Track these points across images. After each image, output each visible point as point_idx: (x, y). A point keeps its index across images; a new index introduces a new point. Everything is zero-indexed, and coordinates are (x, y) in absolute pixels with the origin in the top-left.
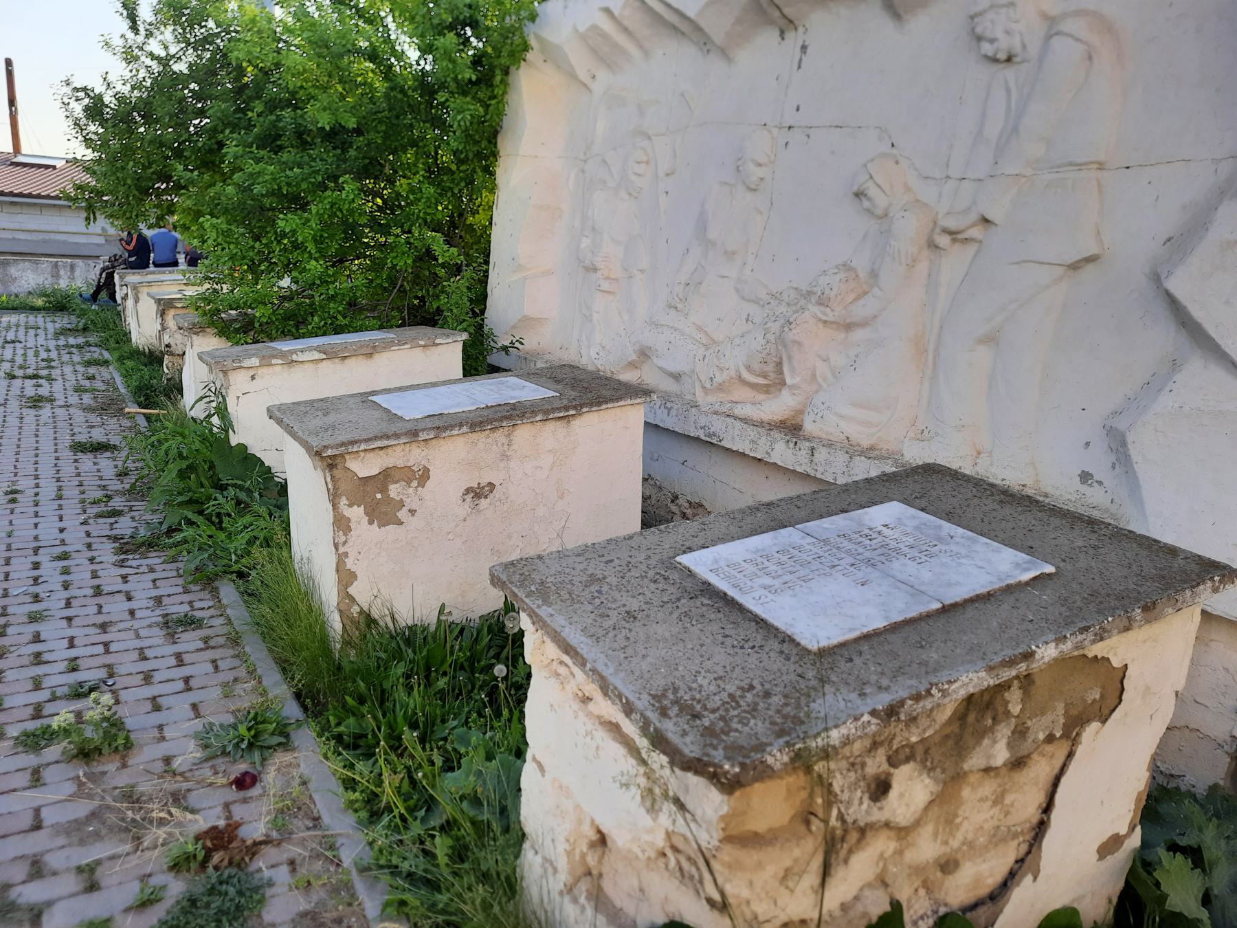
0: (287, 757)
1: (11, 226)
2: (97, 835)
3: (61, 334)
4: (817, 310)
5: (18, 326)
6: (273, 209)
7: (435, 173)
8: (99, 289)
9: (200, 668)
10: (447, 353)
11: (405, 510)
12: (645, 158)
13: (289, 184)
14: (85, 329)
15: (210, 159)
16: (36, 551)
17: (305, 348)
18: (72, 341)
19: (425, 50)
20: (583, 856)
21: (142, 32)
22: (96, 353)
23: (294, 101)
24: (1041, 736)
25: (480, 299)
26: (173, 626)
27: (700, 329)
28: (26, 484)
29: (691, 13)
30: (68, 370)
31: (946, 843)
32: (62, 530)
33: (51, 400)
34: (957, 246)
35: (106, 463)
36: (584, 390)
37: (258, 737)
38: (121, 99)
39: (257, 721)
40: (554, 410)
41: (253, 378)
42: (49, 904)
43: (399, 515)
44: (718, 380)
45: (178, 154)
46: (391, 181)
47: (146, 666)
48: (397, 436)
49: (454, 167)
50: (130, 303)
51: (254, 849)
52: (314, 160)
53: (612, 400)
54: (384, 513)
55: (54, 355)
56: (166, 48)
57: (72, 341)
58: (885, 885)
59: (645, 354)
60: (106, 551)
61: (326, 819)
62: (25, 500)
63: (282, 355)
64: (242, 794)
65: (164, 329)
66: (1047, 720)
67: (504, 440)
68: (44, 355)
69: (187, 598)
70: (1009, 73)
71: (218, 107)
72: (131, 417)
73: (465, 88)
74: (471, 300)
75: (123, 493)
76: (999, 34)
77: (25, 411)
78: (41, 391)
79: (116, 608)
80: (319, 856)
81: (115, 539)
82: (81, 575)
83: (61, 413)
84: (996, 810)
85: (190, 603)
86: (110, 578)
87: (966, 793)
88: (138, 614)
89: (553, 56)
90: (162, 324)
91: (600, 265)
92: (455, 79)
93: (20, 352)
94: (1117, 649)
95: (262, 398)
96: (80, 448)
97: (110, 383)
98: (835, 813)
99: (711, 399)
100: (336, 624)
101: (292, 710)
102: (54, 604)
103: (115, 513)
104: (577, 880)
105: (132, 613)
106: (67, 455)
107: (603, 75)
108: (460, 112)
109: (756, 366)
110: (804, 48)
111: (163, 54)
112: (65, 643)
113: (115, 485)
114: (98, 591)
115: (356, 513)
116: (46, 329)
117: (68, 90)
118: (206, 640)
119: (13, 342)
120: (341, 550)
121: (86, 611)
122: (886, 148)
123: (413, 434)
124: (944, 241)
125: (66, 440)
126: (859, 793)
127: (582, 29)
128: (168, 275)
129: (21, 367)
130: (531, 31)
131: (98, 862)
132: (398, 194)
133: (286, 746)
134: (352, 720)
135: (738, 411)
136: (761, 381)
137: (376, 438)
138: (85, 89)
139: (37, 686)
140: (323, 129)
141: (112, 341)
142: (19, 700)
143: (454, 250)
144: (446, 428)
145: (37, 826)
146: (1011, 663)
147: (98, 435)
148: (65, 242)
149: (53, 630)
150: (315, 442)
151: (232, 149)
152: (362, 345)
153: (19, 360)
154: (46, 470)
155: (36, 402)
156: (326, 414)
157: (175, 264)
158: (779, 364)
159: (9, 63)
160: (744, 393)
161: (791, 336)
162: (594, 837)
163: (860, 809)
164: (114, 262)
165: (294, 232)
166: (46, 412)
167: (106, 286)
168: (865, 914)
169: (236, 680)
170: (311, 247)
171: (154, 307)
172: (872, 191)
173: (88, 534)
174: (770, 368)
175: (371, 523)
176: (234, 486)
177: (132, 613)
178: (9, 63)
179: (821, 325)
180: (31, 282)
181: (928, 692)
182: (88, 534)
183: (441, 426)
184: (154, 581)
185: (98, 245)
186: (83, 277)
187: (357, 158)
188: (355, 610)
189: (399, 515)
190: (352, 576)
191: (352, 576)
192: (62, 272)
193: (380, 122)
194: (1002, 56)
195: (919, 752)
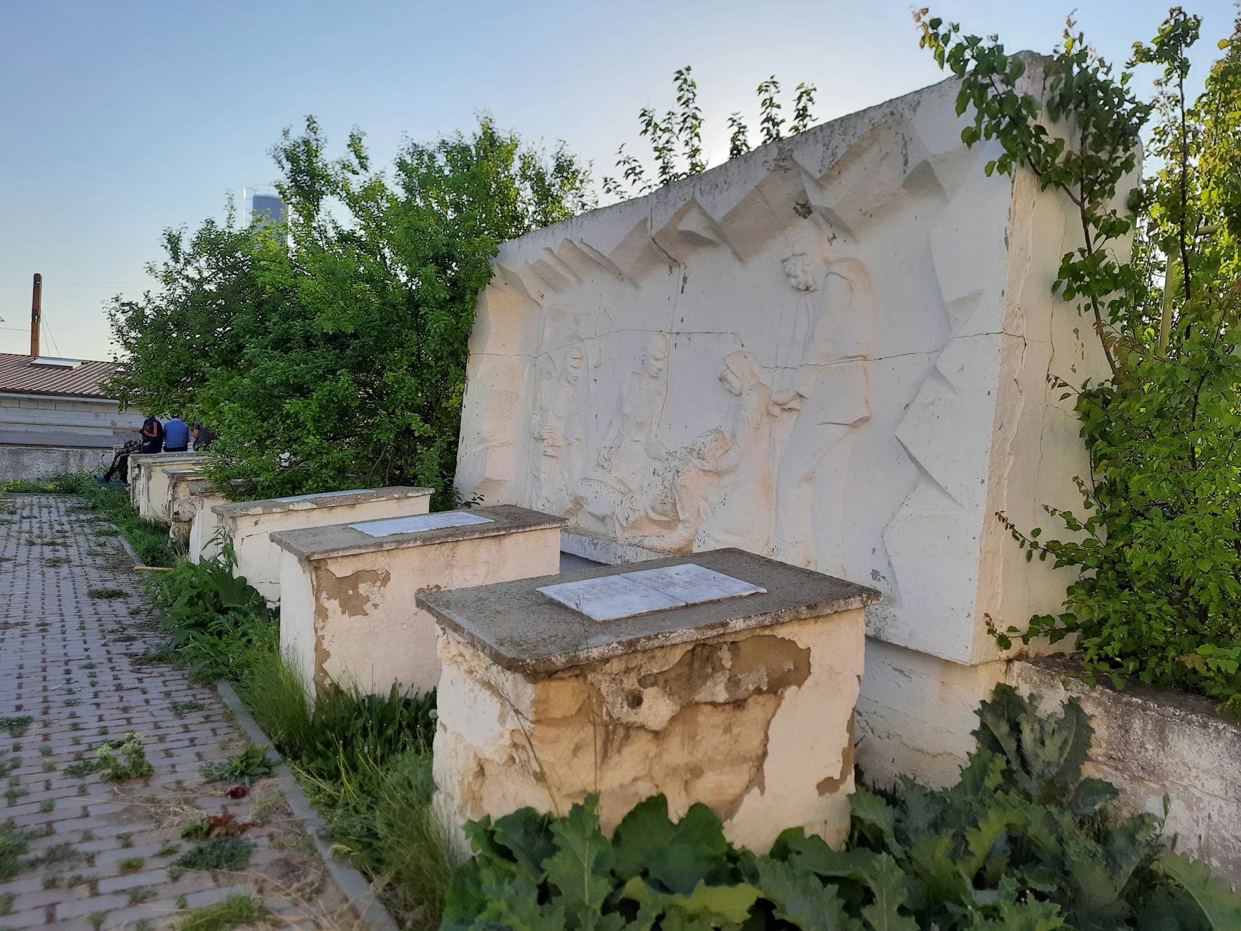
0: (270, 781)
1: (26, 420)
2: (130, 821)
3: (72, 511)
4: (697, 462)
5: (32, 505)
6: (279, 397)
7: (417, 368)
8: (113, 470)
9: (203, 733)
10: (419, 501)
11: (370, 604)
12: (579, 355)
13: (295, 376)
14: (94, 508)
15: (231, 358)
16: (66, 663)
17: (300, 503)
18: (82, 517)
19: (411, 275)
20: (470, 784)
21: (182, 261)
22: (106, 526)
23: (303, 314)
24: (751, 688)
25: (449, 466)
26: (178, 710)
27: (620, 481)
28: (54, 619)
29: (606, 255)
30: (81, 539)
31: (691, 753)
32: (86, 650)
33: (68, 561)
34: (786, 414)
35: (119, 606)
36: (517, 520)
37: (249, 769)
38: (158, 310)
39: (247, 757)
40: (488, 530)
41: (256, 523)
42: (99, 852)
43: (365, 607)
44: (632, 519)
45: (205, 355)
46: (380, 374)
47: (160, 732)
48: (366, 546)
49: (433, 363)
50: (141, 484)
51: (244, 828)
52: (317, 358)
53: (534, 524)
54: (353, 606)
55: (67, 527)
56: (200, 273)
57: (82, 517)
58: (652, 778)
59: (578, 503)
60: (124, 664)
61: (297, 812)
62: (55, 628)
63: (282, 506)
64: (235, 801)
65: (174, 499)
66: (754, 676)
67: (448, 552)
68: (58, 528)
69: (190, 692)
70: (808, 297)
71: (243, 319)
72: (139, 572)
73: (442, 305)
74: (440, 465)
75: (135, 626)
76: (799, 273)
77: (45, 569)
78: (58, 554)
79: (135, 698)
80: (291, 832)
81: (131, 656)
82: (105, 677)
83: (77, 571)
84: (727, 737)
85: (194, 696)
86: (129, 679)
87: (701, 718)
88: (152, 702)
89: (511, 280)
90: (173, 495)
91: (545, 436)
92: (434, 298)
93: (36, 525)
94: (803, 635)
95: (262, 546)
96: (96, 595)
97: (120, 550)
98: (605, 710)
99: (626, 535)
100: (311, 691)
101: (274, 756)
102: (86, 695)
103: (131, 639)
104: (465, 803)
105: (147, 701)
106: (86, 602)
107: (549, 294)
108: (437, 321)
109: (658, 507)
110: (685, 279)
111: (197, 277)
112: (96, 718)
113: (128, 621)
114: (119, 688)
115: (333, 605)
116: (58, 508)
117: (117, 305)
118: (207, 717)
119: (29, 517)
120: (320, 633)
121: (110, 699)
122: (739, 347)
123: (379, 546)
124: (776, 410)
125: (83, 589)
126: (620, 700)
127: (531, 262)
128: (177, 457)
129: (39, 537)
130: (493, 261)
131: (132, 834)
132: (385, 384)
133: (268, 775)
134: (320, 760)
135: (646, 543)
136: (663, 518)
137: (351, 548)
138: (129, 304)
139: (77, 742)
140: (327, 333)
141: (120, 516)
142: (65, 750)
143: (427, 426)
144: (403, 542)
145: (86, 815)
146: (712, 627)
147: (111, 586)
148: (74, 434)
149: (86, 714)
150: (306, 551)
151: (250, 350)
152: (347, 498)
153: (36, 532)
154: (69, 610)
155: (55, 563)
156: (315, 535)
157: (185, 448)
158: (674, 504)
159: (37, 278)
160: (655, 530)
161: (678, 481)
162: (474, 766)
163: (623, 712)
164: (129, 448)
165: (297, 413)
166: (64, 570)
167: (120, 469)
168: (636, 794)
169: (231, 740)
170: (310, 425)
171: (168, 481)
172: (730, 377)
173: (108, 652)
174: (668, 507)
175: (343, 613)
176: (234, 609)
177: (147, 701)
178: (37, 278)
179: (701, 473)
180: (42, 469)
181: (656, 636)
182: (108, 652)
183: (400, 541)
184: (164, 682)
185: (106, 437)
186: (94, 464)
187: (352, 356)
188: (327, 682)
189: (365, 607)
190: (327, 655)
191: (327, 655)
192: (72, 461)
193: (373, 328)
194: (802, 287)
195: (661, 680)
